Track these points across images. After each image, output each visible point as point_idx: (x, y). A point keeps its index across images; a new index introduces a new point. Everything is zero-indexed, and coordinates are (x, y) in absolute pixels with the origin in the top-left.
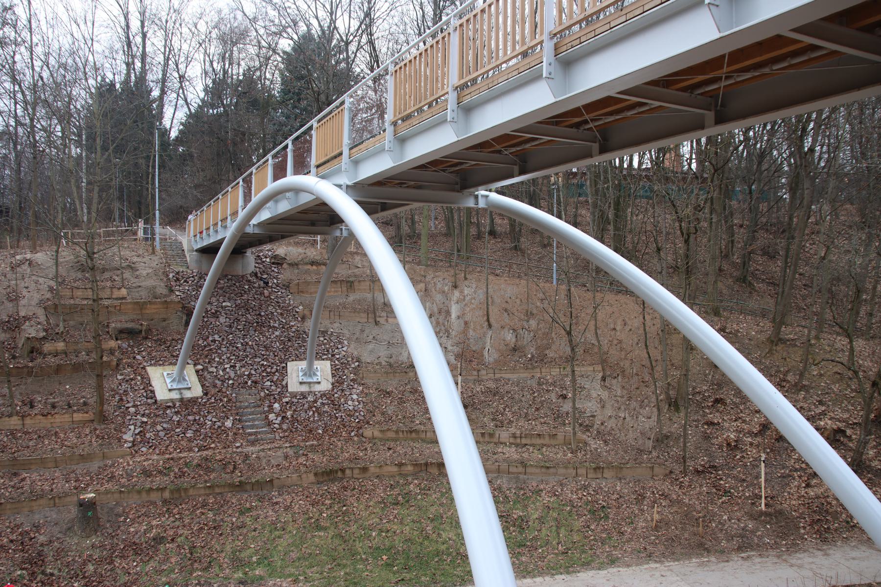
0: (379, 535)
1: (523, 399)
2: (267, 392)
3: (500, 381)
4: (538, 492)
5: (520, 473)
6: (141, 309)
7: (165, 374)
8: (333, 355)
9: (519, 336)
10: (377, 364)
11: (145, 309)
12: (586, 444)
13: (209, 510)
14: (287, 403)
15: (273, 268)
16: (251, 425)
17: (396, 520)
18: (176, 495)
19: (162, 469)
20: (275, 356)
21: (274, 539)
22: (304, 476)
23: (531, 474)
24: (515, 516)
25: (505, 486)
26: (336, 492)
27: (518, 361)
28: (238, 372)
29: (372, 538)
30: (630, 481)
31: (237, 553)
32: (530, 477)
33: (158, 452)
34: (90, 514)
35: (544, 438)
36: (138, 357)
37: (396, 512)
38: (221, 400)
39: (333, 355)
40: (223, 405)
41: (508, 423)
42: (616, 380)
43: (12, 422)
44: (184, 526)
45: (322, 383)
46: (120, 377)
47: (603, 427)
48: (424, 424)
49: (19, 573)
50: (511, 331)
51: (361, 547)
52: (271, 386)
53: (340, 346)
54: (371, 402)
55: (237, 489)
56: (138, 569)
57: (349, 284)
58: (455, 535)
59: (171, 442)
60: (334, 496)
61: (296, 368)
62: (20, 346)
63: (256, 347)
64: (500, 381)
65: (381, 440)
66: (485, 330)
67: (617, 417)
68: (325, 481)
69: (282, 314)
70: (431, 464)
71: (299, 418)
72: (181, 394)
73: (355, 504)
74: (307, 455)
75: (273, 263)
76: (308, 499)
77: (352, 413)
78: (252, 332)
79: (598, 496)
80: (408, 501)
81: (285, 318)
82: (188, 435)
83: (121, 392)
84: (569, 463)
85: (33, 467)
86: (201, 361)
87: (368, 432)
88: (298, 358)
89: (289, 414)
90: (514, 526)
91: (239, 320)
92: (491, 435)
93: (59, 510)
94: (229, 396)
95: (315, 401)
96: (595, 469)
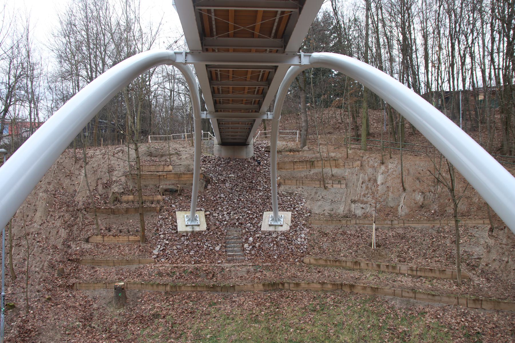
0: (295, 331)
1: (424, 243)
2: (247, 230)
4: (423, 314)
5: (411, 297)
6: (179, 178)
7: (185, 216)
8: (294, 208)
9: (426, 197)
10: (322, 215)
11: (182, 177)
12: (470, 280)
13: (191, 301)
14: (258, 237)
15: (265, 154)
16: (232, 250)
17: (310, 322)
18: (174, 290)
19: (170, 273)
20: (257, 208)
21: (225, 325)
22: (256, 285)
23: (420, 299)
24: (400, 330)
25: (397, 306)
26: (276, 298)
27: (424, 215)
28: (232, 217)
29: (289, 333)
30: (507, 315)
31: (200, 331)
32: (419, 301)
33: (170, 262)
34: (120, 294)
35: (435, 272)
36: (173, 206)
37: (312, 316)
38: (217, 233)
39: (294, 208)
40: (217, 237)
41: (409, 260)
42: (502, 231)
43: (98, 239)
44: (173, 309)
46: (160, 217)
47: (487, 268)
49: (78, 323)
50: (420, 194)
51: (280, 339)
52: (250, 226)
53: (299, 203)
54: (314, 240)
55: (212, 289)
56: (139, 332)
57: (311, 163)
58: (350, 339)
59: (180, 257)
60: (272, 300)
61: (269, 215)
62: (110, 197)
63: (245, 202)
65: (314, 265)
66: (401, 192)
67: (501, 260)
68: (270, 290)
69: (266, 182)
70: (345, 285)
72: (193, 228)
73: (286, 308)
74: (262, 272)
75: (266, 151)
76: (256, 301)
78: (245, 193)
79: (475, 323)
80: (322, 310)
81: (267, 185)
82: (191, 254)
83: (159, 225)
84: (452, 293)
85: (102, 264)
86: (210, 210)
87: (307, 260)
88: (271, 209)
90: (398, 338)
92: (394, 268)
93: (108, 291)
94: (223, 231)
95: (277, 237)
96: (474, 300)
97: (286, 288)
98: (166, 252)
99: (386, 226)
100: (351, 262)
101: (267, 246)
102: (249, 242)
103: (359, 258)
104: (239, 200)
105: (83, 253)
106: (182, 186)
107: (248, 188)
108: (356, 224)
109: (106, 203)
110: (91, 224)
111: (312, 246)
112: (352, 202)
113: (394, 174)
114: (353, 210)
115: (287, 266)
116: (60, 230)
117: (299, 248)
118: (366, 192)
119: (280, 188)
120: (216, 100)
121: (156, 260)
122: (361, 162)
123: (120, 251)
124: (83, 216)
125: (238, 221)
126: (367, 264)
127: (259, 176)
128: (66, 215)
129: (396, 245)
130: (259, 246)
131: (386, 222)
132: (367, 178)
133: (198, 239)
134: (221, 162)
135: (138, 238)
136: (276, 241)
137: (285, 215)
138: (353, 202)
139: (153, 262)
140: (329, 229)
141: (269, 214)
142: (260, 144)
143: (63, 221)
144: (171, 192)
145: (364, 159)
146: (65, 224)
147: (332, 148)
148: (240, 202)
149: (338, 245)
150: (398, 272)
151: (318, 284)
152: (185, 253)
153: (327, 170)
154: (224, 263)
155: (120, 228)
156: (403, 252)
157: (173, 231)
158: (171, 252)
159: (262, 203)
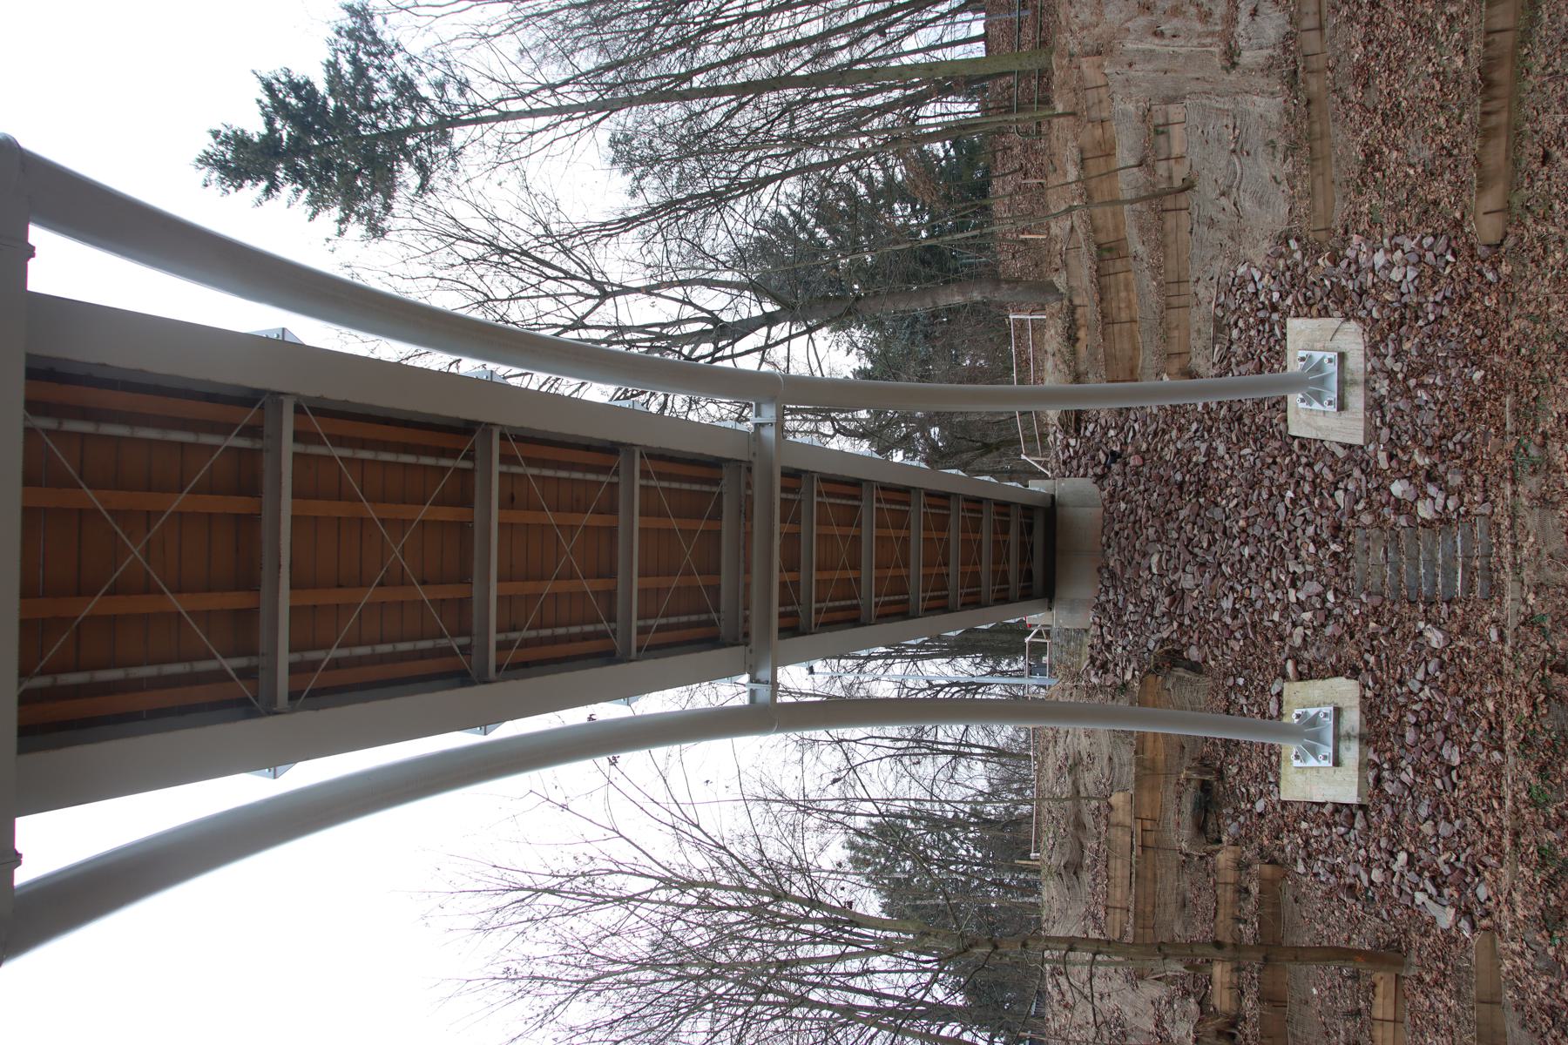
2: (1361, 506)
7: (1297, 763)
10: (1293, 188)
11: (1153, 761)
14: (1391, 457)
15: (1088, 434)
16: (1445, 575)
20: (1274, 462)
28: (1310, 568)
33: (1493, 861)
36: (1260, 806)
38: (1373, 636)
40: (1386, 636)
45: (1344, 347)
46: (1301, 868)
52: (1346, 490)
53: (1251, 288)
54: (1396, 208)
57: (1106, 255)
59: (1471, 813)
63: (1252, 511)
65: (1514, 187)
69: (1180, 430)
72: (1349, 737)
74: (1544, 435)
75: (1077, 431)
78: (1218, 514)
83: (1333, 880)
86: (1279, 660)
87: (1486, 228)
88: (1280, 405)
89: (1422, 461)
91: (1190, 540)
95: (1391, 375)
98: (1446, 870)
102: (1411, 499)
106: (1187, 762)
107: (1202, 500)
108: (1321, 28)
111: (1426, 212)
112: (1234, 65)
119: (1201, 370)
121: (1485, 922)
122: (1087, 54)
127: (1160, 458)
130: (1428, 451)
132: (1142, 21)
133: (1392, 719)
134: (1108, 601)
135: (1383, 981)
136: (1405, 379)
137: (1301, 344)
138: (1231, 58)
139: (1493, 941)
140: (1346, 146)
141: (1297, 412)
144: (1207, 811)
145: (1076, 50)
147: (1053, 180)
148: (1250, 531)
149: (1414, 90)
152: (1454, 786)
153: (1128, 182)
154: (1500, 611)
157: (1357, 825)
158: (1446, 849)
159: (1255, 442)
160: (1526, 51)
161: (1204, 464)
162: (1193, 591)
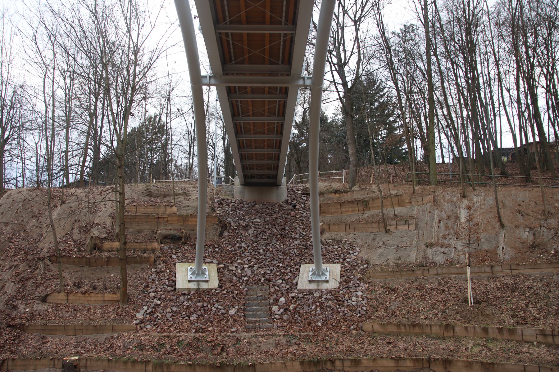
1: (550, 295)
2: (277, 288)
3: (519, 277)
7: (189, 268)
8: (344, 260)
9: (537, 234)
10: (385, 266)
11: (188, 221)
14: (293, 297)
15: (302, 197)
16: (253, 315)
20: (292, 260)
22: (289, 364)
28: (256, 272)
33: (159, 330)
36: (174, 256)
38: (232, 292)
39: (344, 260)
43: (60, 298)
45: (330, 282)
46: (153, 270)
48: (430, 319)
50: (528, 230)
52: (282, 283)
53: (351, 252)
54: (376, 298)
57: (364, 204)
63: (275, 253)
64: (519, 277)
65: (381, 334)
69: (303, 229)
70: (435, 360)
71: (301, 312)
72: (199, 285)
75: (303, 194)
77: (354, 309)
78: (274, 241)
83: (150, 280)
86: (224, 262)
88: (311, 262)
89: (291, 307)
92: (512, 332)
94: (242, 289)
95: (320, 297)
97: (338, 368)
98: (155, 316)
99: (484, 275)
100: (440, 326)
101: (306, 308)
103: (450, 321)
104: (267, 250)
105: (32, 316)
106: (188, 232)
107: (279, 236)
108: (437, 274)
109: (80, 251)
110: (54, 279)
111: (374, 308)
112: (427, 246)
113: (482, 209)
114: (431, 257)
115: (338, 336)
116: (7, 284)
117: (354, 311)
118: (447, 233)
119: (324, 236)
120: (241, 154)
121: (139, 328)
122: (434, 197)
123: (88, 315)
124: (45, 268)
125: (264, 277)
126: (466, 328)
127: (294, 222)
128: (22, 265)
129: (506, 300)
130: (295, 309)
131: (483, 269)
132: (444, 216)
133: (205, 298)
134: (244, 205)
135: (117, 297)
136: (319, 302)
137: (332, 268)
139: (133, 330)
140: (398, 283)
142: (295, 187)
143: (14, 273)
144: (172, 239)
145: (436, 194)
146: (16, 276)
147: (391, 186)
149: (414, 303)
150: (520, 339)
151: (391, 361)
152: (183, 318)
153: (389, 211)
154: (241, 331)
155: (94, 284)
156: (519, 310)
157: (169, 288)
158: (162, 316)
159: (299, 254)
160: (424, 336)
161: (291, 237)
162: (248, 233)
